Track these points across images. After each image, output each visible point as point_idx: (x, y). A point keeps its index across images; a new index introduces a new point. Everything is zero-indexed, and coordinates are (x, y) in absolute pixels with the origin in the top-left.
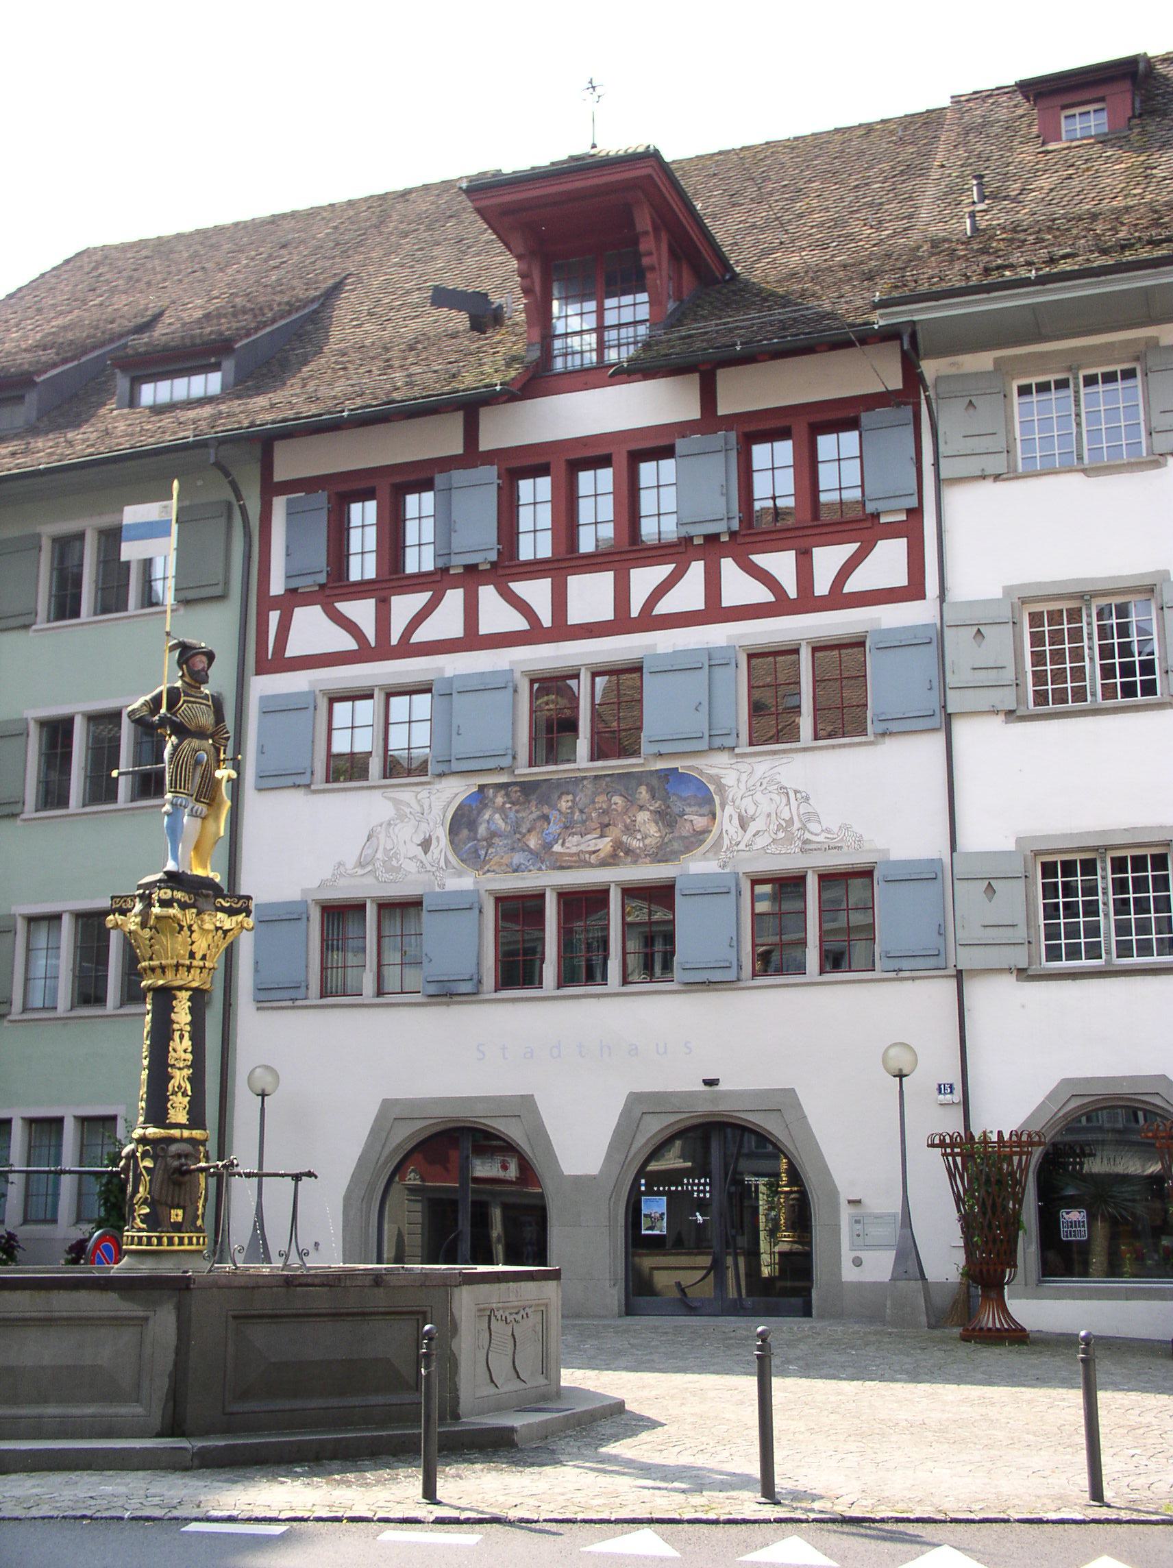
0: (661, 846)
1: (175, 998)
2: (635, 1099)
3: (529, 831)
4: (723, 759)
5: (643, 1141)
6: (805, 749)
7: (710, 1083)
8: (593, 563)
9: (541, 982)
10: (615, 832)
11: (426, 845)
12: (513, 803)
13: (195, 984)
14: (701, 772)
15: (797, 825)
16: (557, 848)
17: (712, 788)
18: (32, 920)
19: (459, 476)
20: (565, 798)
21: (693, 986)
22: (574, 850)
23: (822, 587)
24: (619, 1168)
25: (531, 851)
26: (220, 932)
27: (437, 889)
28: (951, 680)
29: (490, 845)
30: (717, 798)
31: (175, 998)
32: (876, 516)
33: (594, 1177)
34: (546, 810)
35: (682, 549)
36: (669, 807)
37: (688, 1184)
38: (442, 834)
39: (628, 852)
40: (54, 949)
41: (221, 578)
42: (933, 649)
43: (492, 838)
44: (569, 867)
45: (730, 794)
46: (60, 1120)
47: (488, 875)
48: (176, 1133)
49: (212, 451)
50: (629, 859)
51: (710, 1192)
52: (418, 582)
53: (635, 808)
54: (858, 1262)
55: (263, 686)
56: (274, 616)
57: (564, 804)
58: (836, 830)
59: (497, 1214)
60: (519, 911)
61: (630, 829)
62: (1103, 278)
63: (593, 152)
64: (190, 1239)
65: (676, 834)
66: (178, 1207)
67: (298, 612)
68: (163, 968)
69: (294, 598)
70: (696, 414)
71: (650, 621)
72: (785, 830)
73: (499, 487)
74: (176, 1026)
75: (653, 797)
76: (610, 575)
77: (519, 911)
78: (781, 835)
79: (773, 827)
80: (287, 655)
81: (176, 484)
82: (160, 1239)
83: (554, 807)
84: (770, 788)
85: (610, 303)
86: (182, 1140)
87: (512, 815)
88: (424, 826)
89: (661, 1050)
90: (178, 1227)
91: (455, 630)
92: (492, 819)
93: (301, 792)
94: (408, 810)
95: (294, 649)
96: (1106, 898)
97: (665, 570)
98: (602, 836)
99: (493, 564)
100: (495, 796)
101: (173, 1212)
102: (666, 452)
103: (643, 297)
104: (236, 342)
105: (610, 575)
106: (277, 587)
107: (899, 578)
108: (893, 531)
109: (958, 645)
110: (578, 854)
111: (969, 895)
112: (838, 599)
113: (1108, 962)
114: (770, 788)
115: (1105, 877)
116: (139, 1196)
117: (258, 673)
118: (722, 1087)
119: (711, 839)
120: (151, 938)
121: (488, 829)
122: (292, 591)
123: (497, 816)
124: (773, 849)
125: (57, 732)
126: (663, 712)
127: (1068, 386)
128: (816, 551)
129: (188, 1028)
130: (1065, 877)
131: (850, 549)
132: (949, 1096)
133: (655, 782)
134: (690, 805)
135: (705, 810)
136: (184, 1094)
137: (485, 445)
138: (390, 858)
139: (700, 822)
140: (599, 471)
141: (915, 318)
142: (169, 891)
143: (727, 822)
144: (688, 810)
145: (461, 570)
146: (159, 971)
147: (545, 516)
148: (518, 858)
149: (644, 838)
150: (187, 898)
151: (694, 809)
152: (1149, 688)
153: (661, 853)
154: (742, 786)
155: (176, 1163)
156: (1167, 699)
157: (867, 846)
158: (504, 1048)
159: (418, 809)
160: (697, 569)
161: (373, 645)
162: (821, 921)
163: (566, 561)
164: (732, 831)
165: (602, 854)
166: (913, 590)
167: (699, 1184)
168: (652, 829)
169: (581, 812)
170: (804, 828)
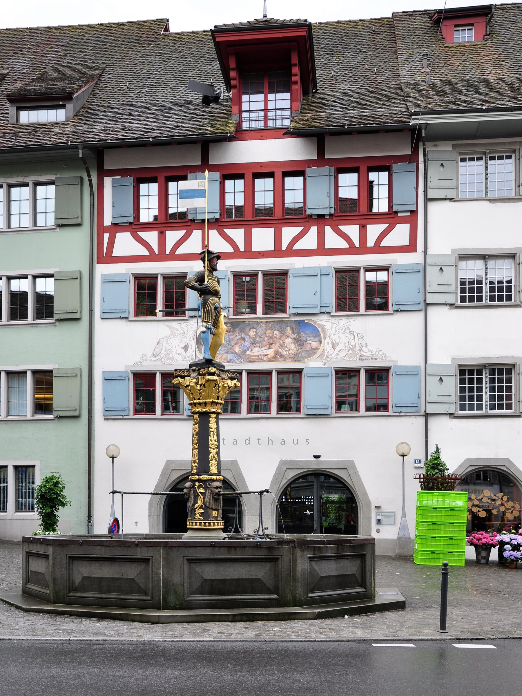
0: (296, 354)
2: (283, 462)
4: (325, 317)
5: (286, 481)
6: (362, 315)
7: (317, 457)
9: (241, 412)
10: (275, 347)
11: (186, 348)
14: (315, 322)
15: (358, 348)
16: (248, 353)
17: (320, 330)
20: (252, 330)
22: (256, 354)
23: (371, 243)
25: (236, 353)
28: (428, 289)
30: (322, 334)
32: (396, 213)
34: (243, 335)
36: (300, 337)
37: (304, 498)
39: (282, 356)
41: (79, 214)
42: (421, 275)
44: (254, 362)
45: (328, 333)
46: (6, 467)
48: (214, 477)
49: (80, 151)
50: (282, 359)
51: (313, 502)
53: (285, 337)
54: (378, 531)
55: (101, 269)
56: (106, 236)
57: (252, 333)
58: (375, 351)
61: (282, 346)
62: (514, 112)
63: (265, 19)
64: (214, 523)
66: (216, 510)
67: (119, 235)
68: (205, 404)
69: (116, 227)
70: (315, 157)
71: (291, 252)
72: (352, 350)
73: (220, 183)
75: (293, 332)
76: (273, 229)
78: (350, 352)
79: (347, 349)
80: (114, 255)
83: (247, 334)
84: (346, 331)
85: (271, 96)
86: (216, 480)
88: (185, 340)
89: (295, 442)
94: (177, 332)
95: (116, 253)
96: (485, 386)
98: (269, 348)
101: (214, 512)
103: (288, 95)
104: (74, 94)
105: (273, 229)
106: (108, 221)
107: (406, 242)
108: (404, 220)
109: (432, 273)
111: (432, 381)
112: (378, 249)
113: (486, 412)
114: (346, 331)
115: (485, 377)
118: (321, 459)
119: (319, 352)
122: (115, 225)
124: (347, 358)
126: (297, 295)
127: (482, 160)
128: (369, 226)
130: (470, 375)
131: (384, 226)
132: (419, 465)
133: (294, 326)
134: (310, 337)
135: (317, 339)
139: (314, 345)
141: (428, 122)
142: (213, 368)
143: (326, 345)
144: (309, 339)
149: (289, 350)
151: (312, 338)
152: (509, 298)
153: (296, 357)
154: (334, 329)
155: (217, 491)
156: (518, 303)
157: (388, 359)
158: (259, 440)
159: (182, 332)
160: (314, 230)
161: (157, 253)
162: (364, 388)
164: (329, 349)
165: (269, 356)
166: (412, 248)
167: (308, 499)
168: (293, 347)
169: (260, 337)
170: (360, 349)
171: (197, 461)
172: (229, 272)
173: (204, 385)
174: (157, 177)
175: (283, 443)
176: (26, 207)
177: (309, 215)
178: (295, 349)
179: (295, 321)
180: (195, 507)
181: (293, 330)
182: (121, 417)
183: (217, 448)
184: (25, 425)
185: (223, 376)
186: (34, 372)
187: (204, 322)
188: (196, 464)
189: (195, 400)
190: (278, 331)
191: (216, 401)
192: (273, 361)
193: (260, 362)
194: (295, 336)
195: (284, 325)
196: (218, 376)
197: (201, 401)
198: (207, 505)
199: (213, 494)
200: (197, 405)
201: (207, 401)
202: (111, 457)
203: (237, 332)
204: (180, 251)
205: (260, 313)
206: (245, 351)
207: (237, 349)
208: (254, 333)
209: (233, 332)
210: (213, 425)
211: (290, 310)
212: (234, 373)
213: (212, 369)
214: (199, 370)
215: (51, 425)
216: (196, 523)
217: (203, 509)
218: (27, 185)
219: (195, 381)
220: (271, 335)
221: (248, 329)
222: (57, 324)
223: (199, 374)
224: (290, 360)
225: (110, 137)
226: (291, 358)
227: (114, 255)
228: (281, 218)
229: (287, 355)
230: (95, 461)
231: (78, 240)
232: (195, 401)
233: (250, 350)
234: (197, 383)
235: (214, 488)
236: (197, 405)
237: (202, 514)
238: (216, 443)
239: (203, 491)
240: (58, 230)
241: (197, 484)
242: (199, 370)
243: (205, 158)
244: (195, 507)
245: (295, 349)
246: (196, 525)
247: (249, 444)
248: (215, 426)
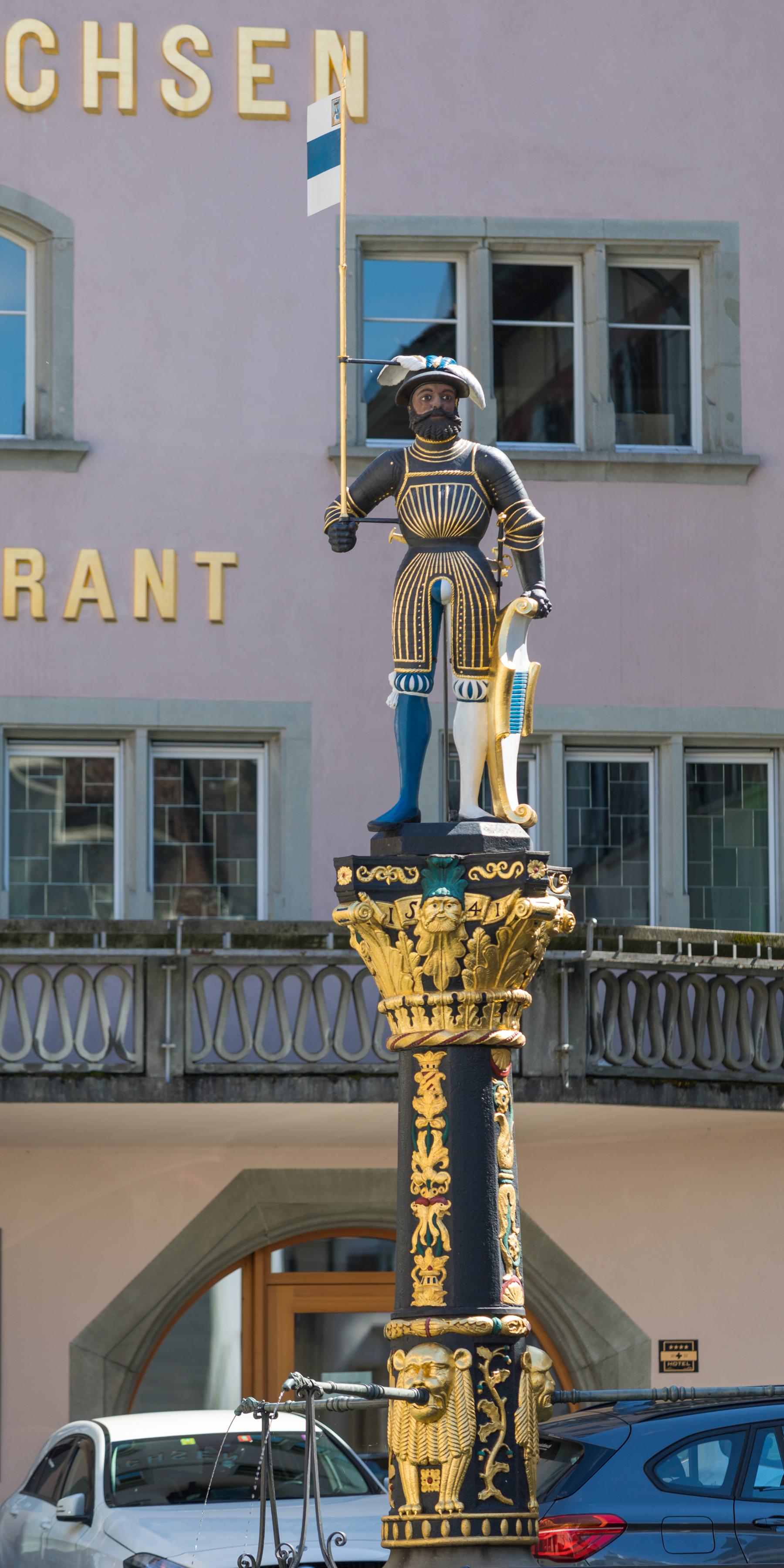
13: (441, 1038)
59: (690, 946)
74: (420, 1123)
129: (440, 1123)
136: (438, 1251)
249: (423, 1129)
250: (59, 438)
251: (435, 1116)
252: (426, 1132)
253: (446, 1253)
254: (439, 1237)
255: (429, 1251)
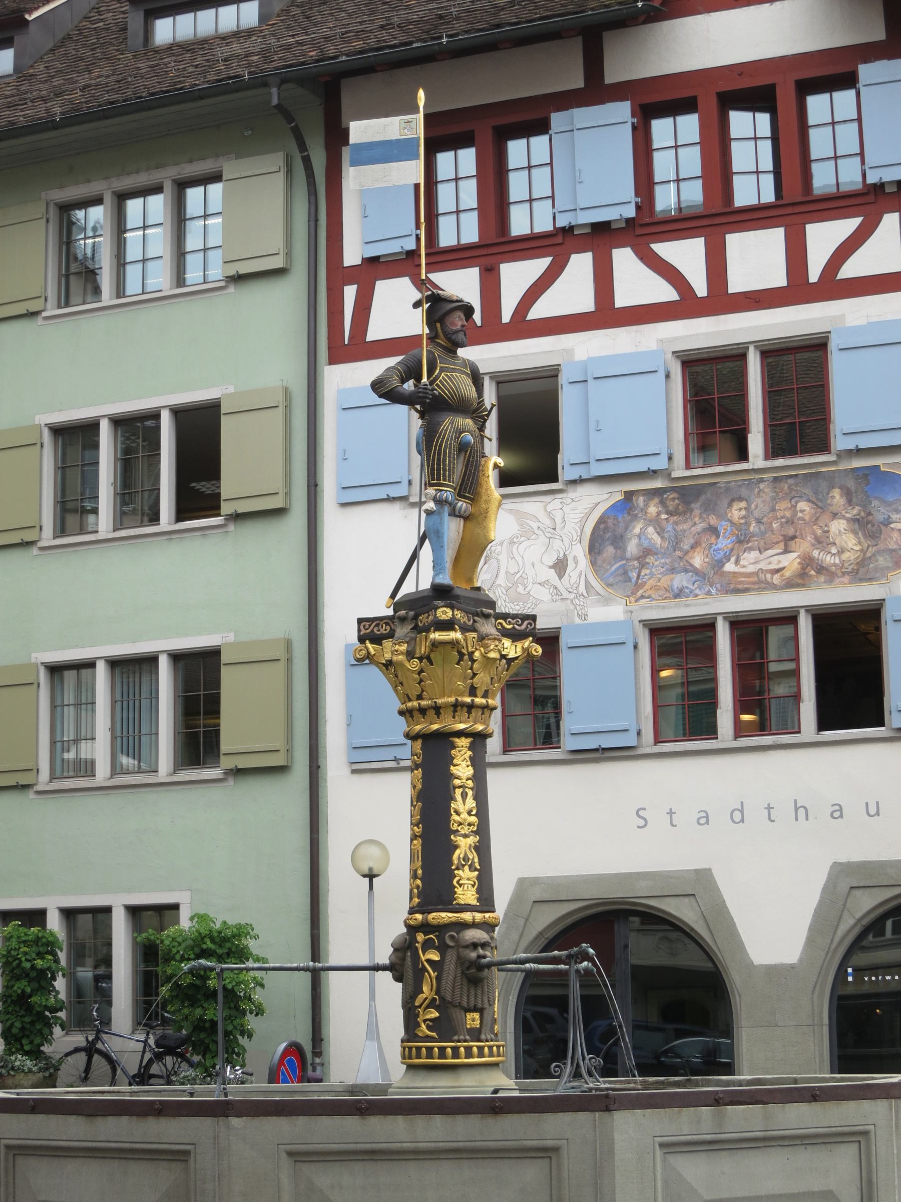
0: (862, 563)
1: (454, 747)
2: (840, 870)
3: (693, 547)
5: (851, 922)
8: (755, 217)
10: (803, 546)
11: (560, 566)
12: (670, 513)
16: (730, 567)
18: (55, 670)
19: (582, 115)
20: (736, 506)
21: (582, 756)
22: (751, 569)
24: (823, 954)
25: (696, 572)
26: (504, 661)
27: (578, 621)
29: (643, 565)
31: (454, 747)
33: (792, 967)
34: (713, 520)
35: (871, 198)
36: (870, 514)
38: (579, 554)
39: (821, 569)
40: (86, 704)
43: (645, 557)
44: (746, 590)
46: (108, 910)
47: (643, 601)
48: (467, 916)
49: (274, 91)
50: (822, 579)
52: (530, 246)
53: (825, 518)
56: (350, 293)
57: (736, 512)
60: (680, 643)
61: (823, 542)
65: (882, 546)
66: (475, 1010)
68: (437, 709)
71: (833, 287)
73: (634, 128)
75: (850, 502)
77: (680, 643)
80: (370, 337)
81: (421, 94)
82: (455, 1050)
83: (722, 517)
86: (474, 925)
87: (669, 528)
88: (557, 544)
89: (873, 811)
90: (476, 1035)
91: (586, 303)
92: (642, 533)
93: (397, 507)
94: (534, 525)
97: (849, 225)
98: (786, 551)
99: (629, 221)
100: (647, 505)
101: (469, 1016)
102: (848, 81)
110: (756, 574)
116: (421, 997)
117: (333, 361)
120: (421, 671)
121: (639, 545)
123: (651, 530)
125: (76, 437)
133: (851, 484)
136: (472, 868)
137: (612, 76)
138: (515, 584)
140: (679, 119)
142: (448, 610)
144: (894, 517)
145: (588, 230)
146: (432, 713)
147: (469, 194)
148: (680, 580)
149: (841, 552)
150: (466, 619)
153: (862, 571)
155: (473, 955)
159: (548, 522)
163: (717, 218)
165: (787, 574)
168: (851, 542)
169: (759, 521)
171: (420, 872)
172: (669, 356)
173: (429, 659)
174: (473, 131)
175: (837, 814)
176: (159, 241)
177: (875, 185)
178: (858, 548)
179: (854, 470)
180: (417, 1004)
181: (848, 495)
182: (392, 764)
183: (475, 833)
184: (150, 796)
185: (488, 628)
186: (177, 657)
187: (431, 485)
188: (419, 882)
189: (410, 700)
190: (809, 500)
191: (468, 700)
192: (798, 585)
193: (764, 589)
194: (855, 512)
195: (824, 485)
196: (465, 629)
197: (424, 703)
198: (449, 998)
199: (462, 964)
200: (416, 715)
201: (440, 701)
202: (364, 876)
203: (697, 512)
204: (539, 311)
205: (756, 456)
206: (720, 564)
207: (698, 560)
208: (743, 513)
209: (685, 513)
210: (462, 769)
211: (840, 443)
212: (523, 620)
213: (444, 613)
214: (415, 618)
215: (216, 793)
216: (419, 1049)
217: (437, 1008)
218: (157, 189)
219: (404, 647)
220: (788, 514)
221: (725, 502)
222: (231, 527)
223: (415, 628)
224: (846, 579)
225: (341, 51)
226: (848, 573)
227: (370, 337)
228: (800, 199)
229: (835, 565)
230: (330, 887)
231: (280, 309)
232: (410, 704)
233: (733, 559)
234: (410, 655)
235: (467, 947)
236: (416, 715)
237: (434, 1025)
238: (474, 819)
239: (435, 956)
240: (231, 289)
241: (420, 937)
242: (415, 618)
243: (594, 65)
244: (417, 1004)
245: (858, 548)
246: (419, 1056)
247: (742, 820)
248: (470, 771)
249: (460, 787)
250: (457, 301)
251: (467, 780)
252: (461, 790)
253: (476, 870)
254: (473, 859)
255: (467, 867)
